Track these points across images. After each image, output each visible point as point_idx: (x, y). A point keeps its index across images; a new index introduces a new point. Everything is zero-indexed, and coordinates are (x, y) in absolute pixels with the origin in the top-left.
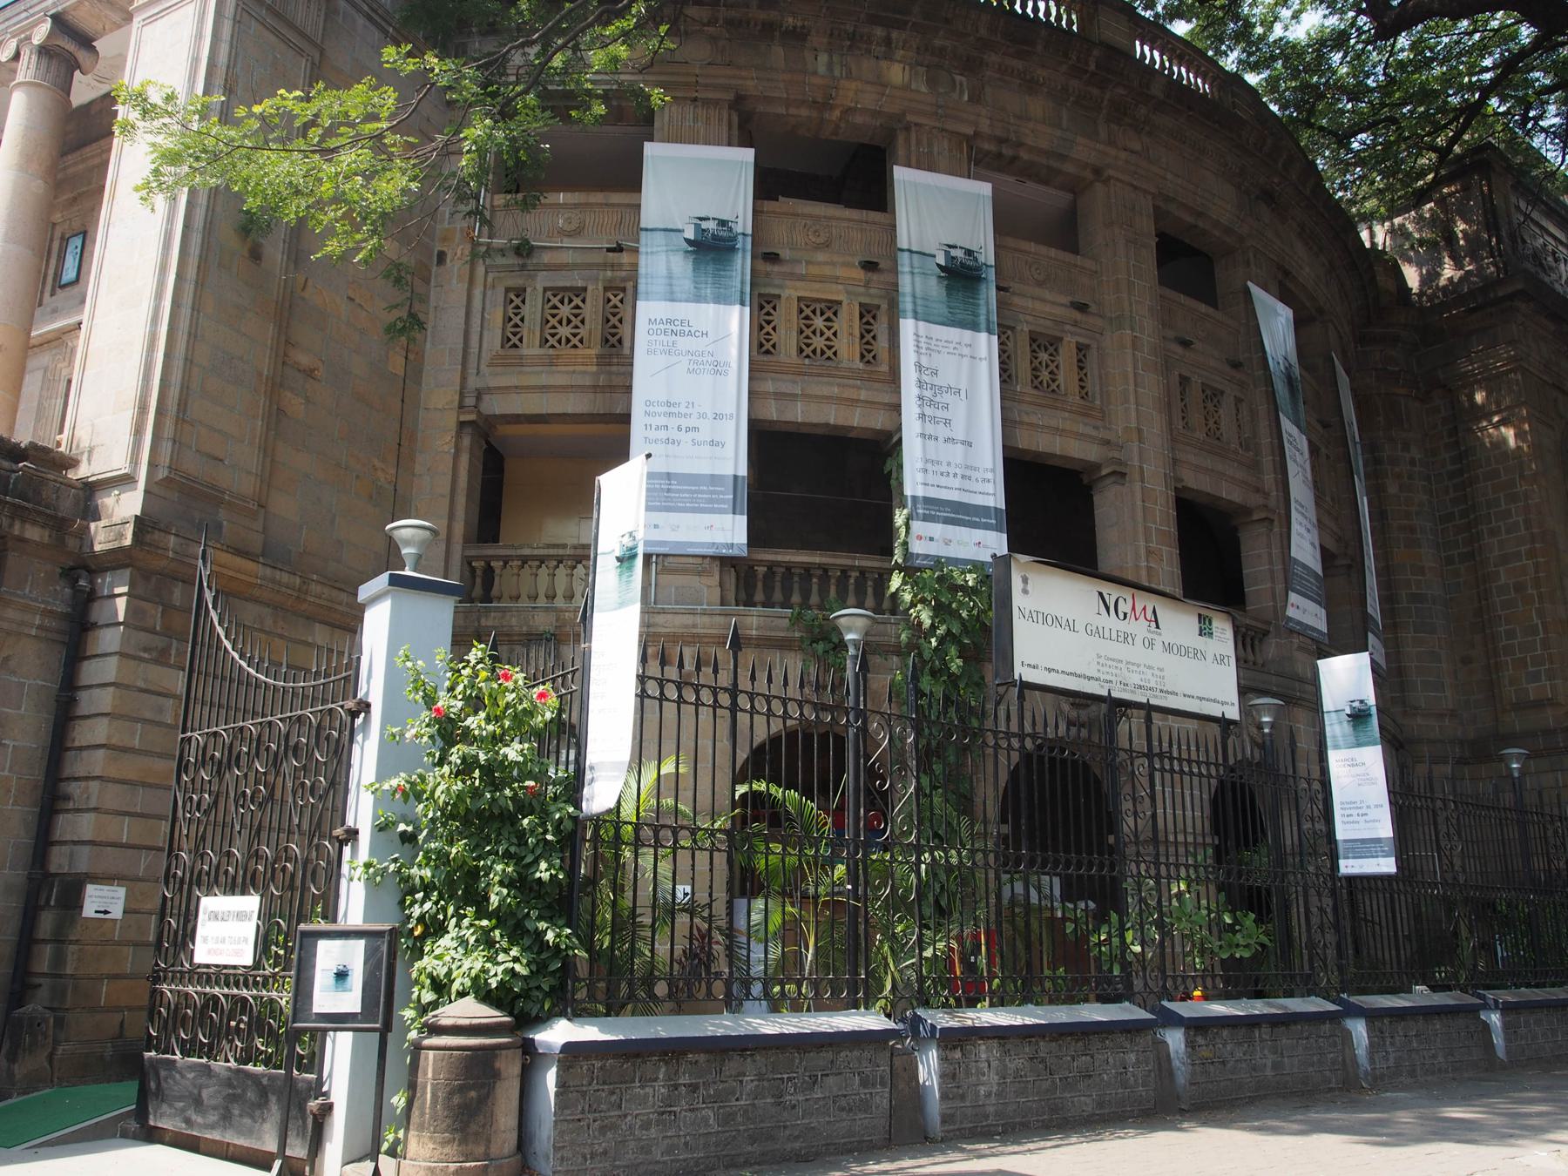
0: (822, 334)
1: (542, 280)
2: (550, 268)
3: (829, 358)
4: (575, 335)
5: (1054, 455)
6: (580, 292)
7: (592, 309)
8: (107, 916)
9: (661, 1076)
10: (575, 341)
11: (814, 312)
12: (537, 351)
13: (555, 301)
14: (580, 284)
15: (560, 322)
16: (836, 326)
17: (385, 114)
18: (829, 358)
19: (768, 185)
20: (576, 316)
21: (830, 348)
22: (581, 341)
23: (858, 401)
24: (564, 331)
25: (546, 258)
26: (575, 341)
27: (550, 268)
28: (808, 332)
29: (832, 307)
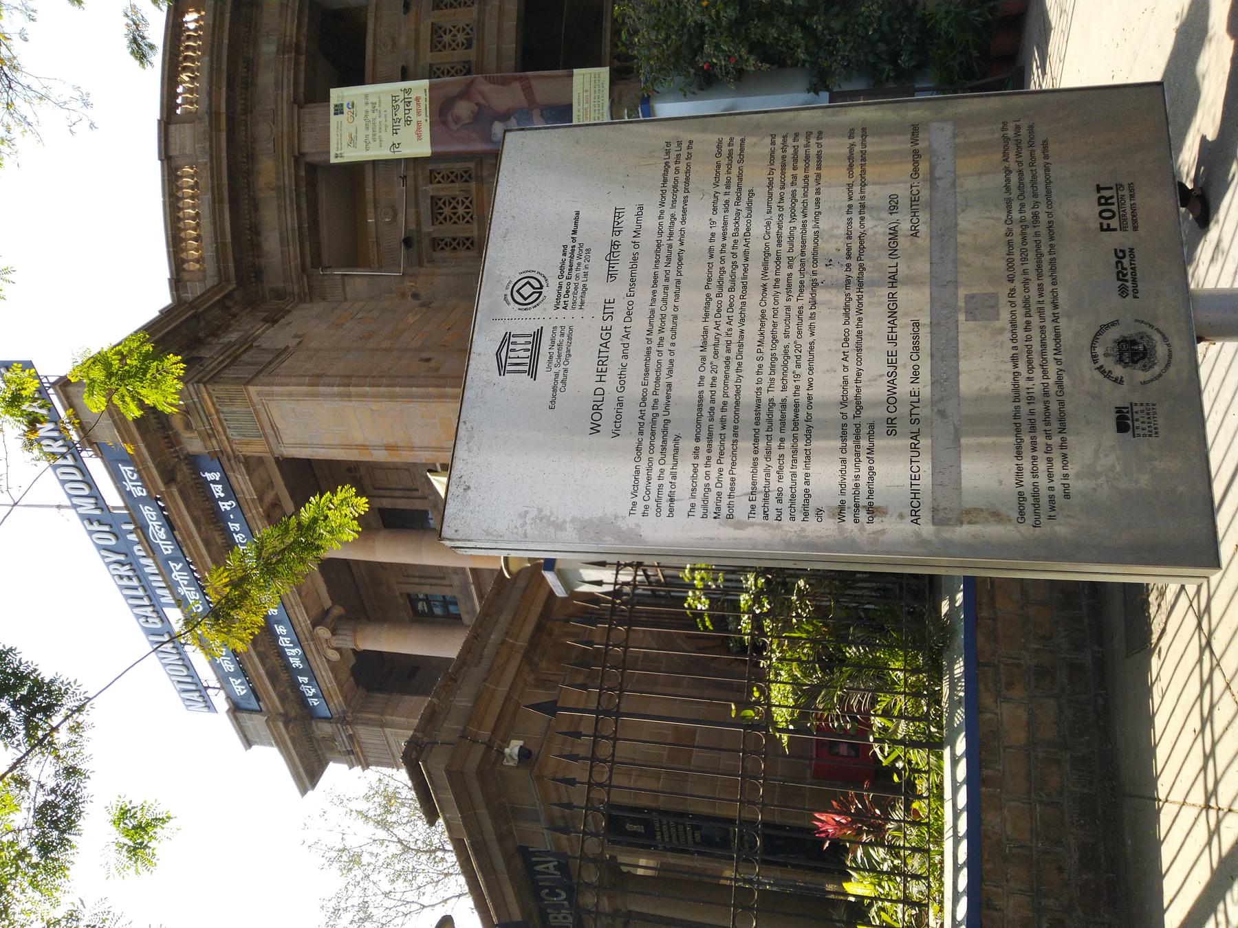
0: (455, 208)
1: (427, 228)
2: (418, 224)
3: (471, 202)
4: (463, 203)
5: (518, 10)
6: (434, 200)
7: (446, 190)
8: (925, 320)
9: (808, 776)
10: (467, 202)
11: (440, 43)
12: (475, 225)
13: (441, 218)
14: (429, 201)
15: (455, 214)
16: (449, 27)
17: (328, 603)
18: (471, 202)
19: (355, 77)
20: (450, 203)
21: (464, 30)
22: (467, 198)
23: (500, 7)
24: (461, 210)
25: (413, 226)
26: (467, 202)
27: (418, 224)
28: (454, 45)
29: (436, 30)
